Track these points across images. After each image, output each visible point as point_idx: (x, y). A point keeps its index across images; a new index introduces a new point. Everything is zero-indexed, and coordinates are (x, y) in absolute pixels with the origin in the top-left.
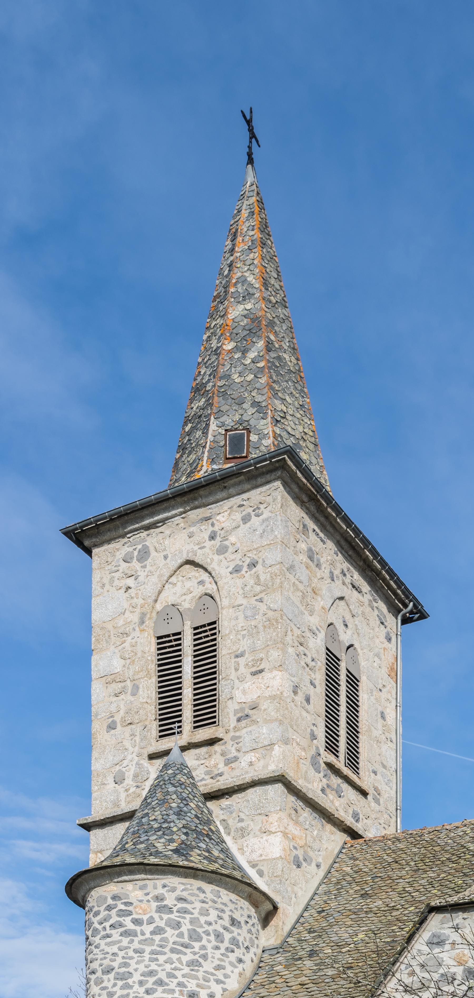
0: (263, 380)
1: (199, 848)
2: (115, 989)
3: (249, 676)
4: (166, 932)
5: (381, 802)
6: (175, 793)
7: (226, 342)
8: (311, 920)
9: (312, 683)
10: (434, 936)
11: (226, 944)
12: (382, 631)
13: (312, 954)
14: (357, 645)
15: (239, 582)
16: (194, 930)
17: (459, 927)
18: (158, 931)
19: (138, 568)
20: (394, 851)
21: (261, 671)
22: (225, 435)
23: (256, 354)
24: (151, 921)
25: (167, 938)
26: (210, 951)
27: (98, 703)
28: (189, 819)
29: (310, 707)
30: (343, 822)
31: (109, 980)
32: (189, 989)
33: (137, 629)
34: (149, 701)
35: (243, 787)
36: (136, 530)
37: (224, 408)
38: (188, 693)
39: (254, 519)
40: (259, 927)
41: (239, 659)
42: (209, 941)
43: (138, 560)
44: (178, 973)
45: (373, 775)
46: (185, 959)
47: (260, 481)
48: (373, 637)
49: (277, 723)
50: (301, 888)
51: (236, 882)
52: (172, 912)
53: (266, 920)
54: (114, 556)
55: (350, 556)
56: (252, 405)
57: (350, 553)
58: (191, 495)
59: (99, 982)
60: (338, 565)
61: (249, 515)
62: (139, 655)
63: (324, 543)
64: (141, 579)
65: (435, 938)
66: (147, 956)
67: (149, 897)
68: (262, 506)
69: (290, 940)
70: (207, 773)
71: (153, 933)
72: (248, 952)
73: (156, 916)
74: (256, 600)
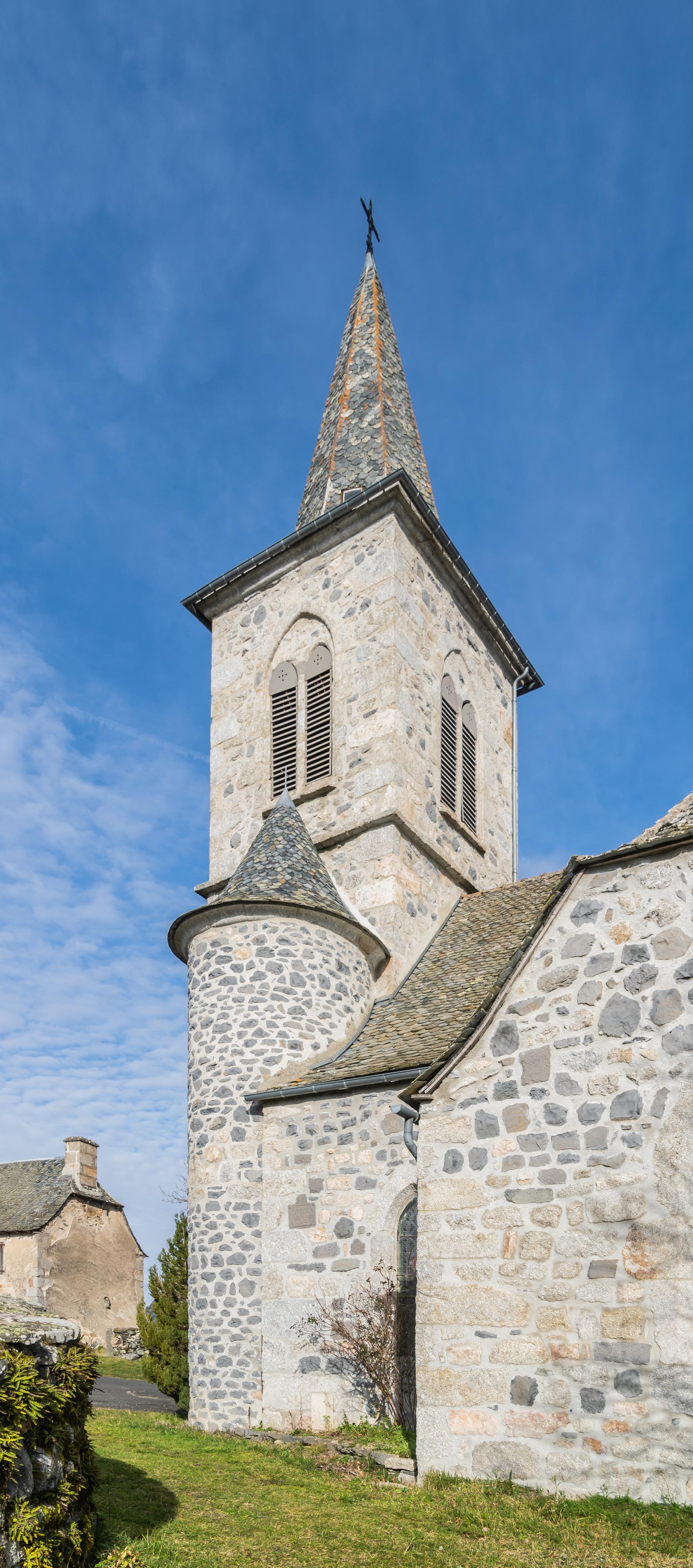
0: (379, 440)
1: (305, 888)
2: (213, 1043)
3: (362, 719)
4: (266, 977)
5: (498, 862)
6: (282, 834)
7: (344, 411)
8: (426, 970)
9: (427, 729)
10: (581, 905)
11: (333, 990)
12: (498, 696)
13: (425, 1002)
14: (473, 702)
15: (352, 625)
16: (297, 974)
17: (617, 888)
18: (259, 976)
19: (255, 630)
20: (512, 899)
21: (374, 712)
22: (341, 495)
23: (373, 417)
24: (251, 966)
25: (267, 984)
26: (314, 997)
27: (216, 769)
28: (295, 860)
29: (425, 753)
30: (459, 874)
31: (208, 1034)
32: (291, 1039)
33: (253, 690)
34: (264, 761)
35: (355, 832)
36: (253, 591)
37: (341, 471)
38: (302, 747)
39: (367, 557)
40: (371, 977)
41: (352, 703)
42: (313, 987)
43: (255, 622)
44: (279, 1022)
45: (489, 835)
46: (287, 1006)
47: (373, 516)
48: (489, 698)
49: (390, 763)
50: (416, 939)
51: (344, 922)
52: (273, 955)
53: (378, 970)
54: (233, 622)
55: (466, 610)
56: (368, 464)
57: (466, 607)
58: (304, 544)
59: (198, 1037)
60: (454, 617)
61: (362, 555)
62: (255, 715)
63: (440, 591)
64: (257, 640)
65: (582, 908)
66: (246, 1004)
67: (249, 940)
68: (375, 544)
69: (403, 991)
70: (319, 825)
71: (253, 979)
72: (358, 1001)
73: (256, 960)
74: (369, 640)
